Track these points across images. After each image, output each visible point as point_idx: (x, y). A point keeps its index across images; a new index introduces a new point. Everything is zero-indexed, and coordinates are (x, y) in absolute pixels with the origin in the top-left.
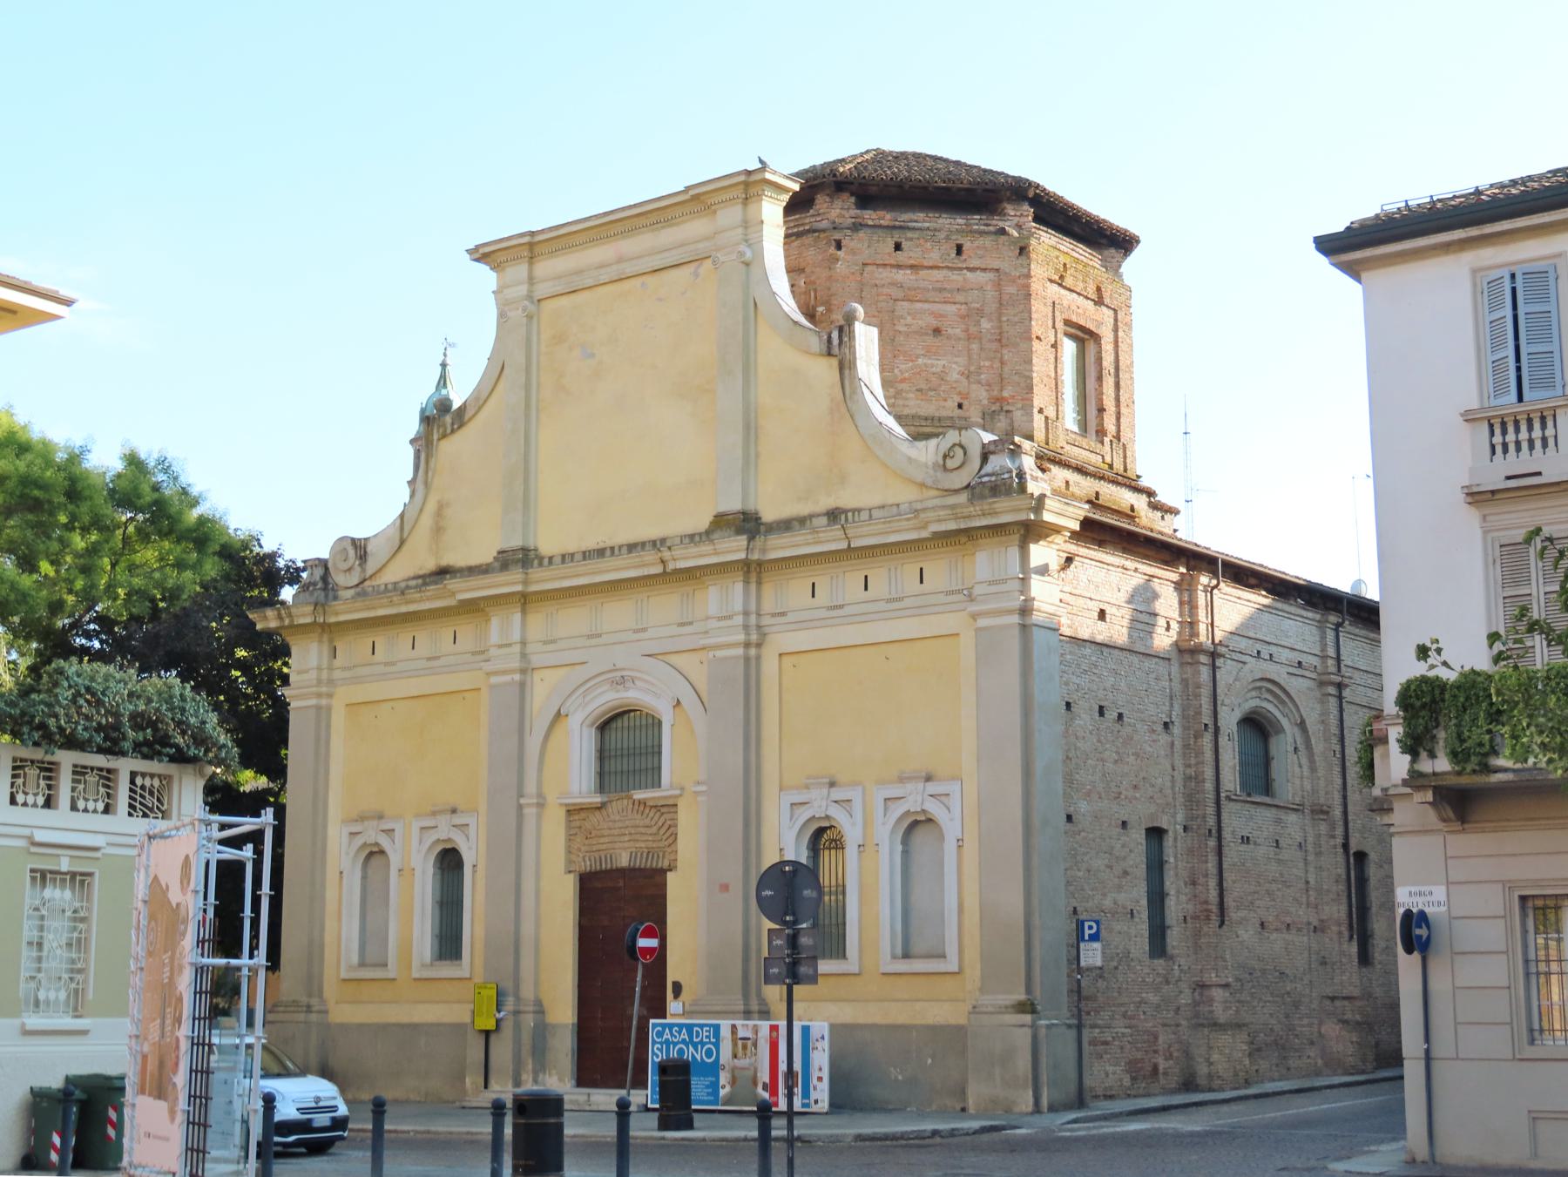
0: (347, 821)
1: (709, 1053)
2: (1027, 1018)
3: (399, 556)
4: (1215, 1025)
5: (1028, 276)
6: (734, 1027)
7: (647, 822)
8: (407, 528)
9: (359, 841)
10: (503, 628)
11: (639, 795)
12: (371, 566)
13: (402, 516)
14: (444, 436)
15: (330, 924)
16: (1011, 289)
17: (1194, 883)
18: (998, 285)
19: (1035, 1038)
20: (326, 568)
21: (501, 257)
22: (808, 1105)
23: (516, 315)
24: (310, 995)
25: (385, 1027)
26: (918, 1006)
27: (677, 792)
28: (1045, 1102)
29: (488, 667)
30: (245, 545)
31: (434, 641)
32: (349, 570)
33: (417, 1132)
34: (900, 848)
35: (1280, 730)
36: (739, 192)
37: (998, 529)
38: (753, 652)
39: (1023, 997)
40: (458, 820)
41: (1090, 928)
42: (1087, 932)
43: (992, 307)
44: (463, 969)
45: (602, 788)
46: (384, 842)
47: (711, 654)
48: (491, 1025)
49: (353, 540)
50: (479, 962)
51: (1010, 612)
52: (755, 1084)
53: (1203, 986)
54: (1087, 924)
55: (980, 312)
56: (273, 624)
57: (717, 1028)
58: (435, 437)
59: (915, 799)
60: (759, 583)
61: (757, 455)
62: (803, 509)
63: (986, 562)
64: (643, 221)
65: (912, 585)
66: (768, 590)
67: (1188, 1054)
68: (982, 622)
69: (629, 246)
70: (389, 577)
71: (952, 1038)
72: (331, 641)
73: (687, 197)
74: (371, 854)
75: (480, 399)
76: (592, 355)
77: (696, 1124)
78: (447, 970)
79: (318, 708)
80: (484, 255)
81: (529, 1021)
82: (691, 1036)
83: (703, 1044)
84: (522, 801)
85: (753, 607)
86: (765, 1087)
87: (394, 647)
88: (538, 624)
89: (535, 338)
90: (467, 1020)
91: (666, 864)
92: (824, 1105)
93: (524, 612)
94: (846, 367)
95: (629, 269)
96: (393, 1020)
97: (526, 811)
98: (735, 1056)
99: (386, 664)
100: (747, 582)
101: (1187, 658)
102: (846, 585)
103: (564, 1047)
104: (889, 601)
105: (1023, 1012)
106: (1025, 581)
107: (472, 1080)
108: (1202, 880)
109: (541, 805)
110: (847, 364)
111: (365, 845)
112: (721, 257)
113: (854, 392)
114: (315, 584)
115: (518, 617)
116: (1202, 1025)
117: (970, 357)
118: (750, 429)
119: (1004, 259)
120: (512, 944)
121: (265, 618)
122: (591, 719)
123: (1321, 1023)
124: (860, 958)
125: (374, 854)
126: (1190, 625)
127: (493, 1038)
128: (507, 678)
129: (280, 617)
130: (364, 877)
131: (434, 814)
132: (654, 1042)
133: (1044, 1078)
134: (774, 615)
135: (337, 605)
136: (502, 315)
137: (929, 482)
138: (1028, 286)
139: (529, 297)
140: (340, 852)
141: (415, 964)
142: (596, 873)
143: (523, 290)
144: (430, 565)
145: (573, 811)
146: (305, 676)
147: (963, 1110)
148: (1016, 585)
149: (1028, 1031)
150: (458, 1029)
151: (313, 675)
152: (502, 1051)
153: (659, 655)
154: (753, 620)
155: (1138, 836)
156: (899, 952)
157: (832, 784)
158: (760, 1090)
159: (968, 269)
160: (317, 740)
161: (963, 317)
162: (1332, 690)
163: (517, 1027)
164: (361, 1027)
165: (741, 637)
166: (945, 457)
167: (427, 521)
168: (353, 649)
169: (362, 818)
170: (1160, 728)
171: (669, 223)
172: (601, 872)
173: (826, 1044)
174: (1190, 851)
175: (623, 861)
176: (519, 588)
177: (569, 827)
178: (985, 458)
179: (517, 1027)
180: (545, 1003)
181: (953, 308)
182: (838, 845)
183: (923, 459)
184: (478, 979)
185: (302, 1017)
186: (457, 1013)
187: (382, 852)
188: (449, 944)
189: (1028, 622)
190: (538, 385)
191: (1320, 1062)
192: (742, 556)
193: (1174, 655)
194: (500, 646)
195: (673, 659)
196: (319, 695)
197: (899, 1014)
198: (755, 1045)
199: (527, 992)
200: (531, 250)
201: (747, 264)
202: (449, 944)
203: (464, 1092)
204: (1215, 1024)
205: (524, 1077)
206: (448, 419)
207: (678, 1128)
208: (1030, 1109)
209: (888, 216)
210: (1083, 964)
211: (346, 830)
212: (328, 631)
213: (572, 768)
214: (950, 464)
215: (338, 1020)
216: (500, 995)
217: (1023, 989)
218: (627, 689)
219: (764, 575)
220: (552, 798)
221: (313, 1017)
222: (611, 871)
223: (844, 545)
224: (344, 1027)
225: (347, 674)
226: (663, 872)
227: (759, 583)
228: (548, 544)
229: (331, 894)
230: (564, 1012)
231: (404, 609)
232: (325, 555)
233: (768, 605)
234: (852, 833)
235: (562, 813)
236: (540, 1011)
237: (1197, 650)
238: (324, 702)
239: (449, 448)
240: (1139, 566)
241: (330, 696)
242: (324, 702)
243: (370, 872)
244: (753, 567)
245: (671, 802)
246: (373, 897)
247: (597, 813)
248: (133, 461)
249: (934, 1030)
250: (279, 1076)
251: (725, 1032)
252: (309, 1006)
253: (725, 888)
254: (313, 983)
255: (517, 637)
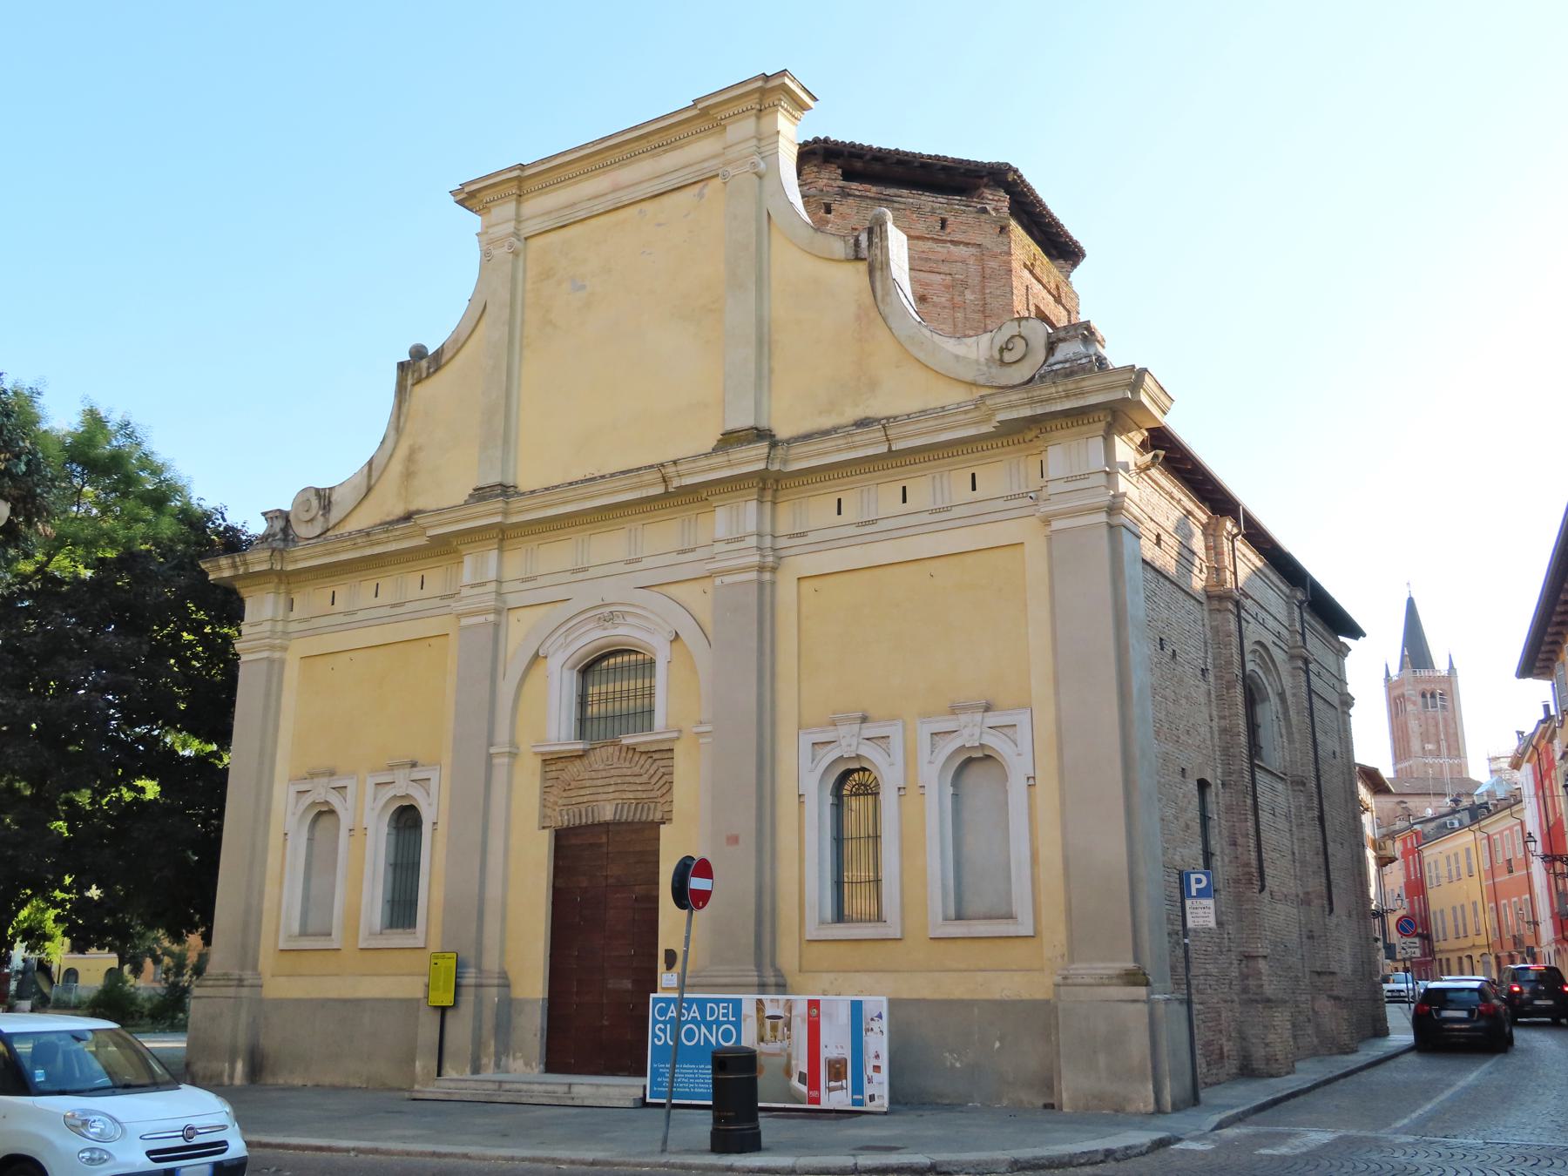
0: (294, 780)
1: (727, 1035)
2: (1141, 992)
3: (366, 503)
4: (1268, 1002)
5: (1010, 254)
6: (760, 1002)
7: (637, 770)
8: (375, 475)
9: (307, 800)
10: (479, 565)
11: (628, 740)
12: (335, 515)
13: (370, 463)
14: (419, 381)
15: (270, 889)
16: (993, 264)
17: (1235, 844)
18: (981, 260)
19: (1152, 1015)
20: (288, 521)
21: (486, 196)
22: (860, 1102)
23: (501, 252)
24: (243, 968)
25: (324, 1003)
26: (980, 977)
27: (675, 735)
28: (1167, 1098)
29: (457, 606)
30: (207, 516)
31: (399, 586)
32: (311, 520)
33: (359, 1151)
34: (950, 790)
35: (1266, 699)
36: (752, 102)
37: (1078, 416)
38: (767, 576)
39: (1131, 965)
40: (417, 774)
41: (1199, 881)
42: (1194, 887)
43: (975, 280)
44: (416, 938)
45: (581, 734)
46: (335, 801)
47: (718, 581)
48: (448, 1000)
49: (317, 490)
50: (436, 931)
51: (1096, 510)
52: (788, 1074)
53: (1249, 957)
54: (1193, 877)
55: (965, 284)
56: (227, 574)
57: (737, 1004)
58: (410, 382)
59: (971, 732)
60: (774, 503)
61: (771, 371)
62: (827, 422)
63: (1065, 457)
64: (644, 145)
65: (963, 492)
66: (784, 510)
67: (1243, 1038)
68: (1057, 525)
69: (626, 174)
70: (353, 525)
71: (1039, 1018)
72: (288, 593)
73: (695, 112)
74: (320, 814)
75: (458, 343)
76: (583, 287)
77: (765, 1139)
78: (399, 939)
79: (271, 661)
80: (470, 197)
81: (493, 995)
82: (703, 1014)
83: (719, 1024)
84: (492, 750)
85: (767, 528)
86: (802, 1078)
87: (356, 594)
88: (516, 562)
89: (520, 276)
90: (420, 994)
91: (658, 816)
92: (883, 1103)
93: (501, 549)
94: (876, 268)
95: (626, 197)
96: (333, 995)
97: (496, 761)
98: (762, 1039)
99: (346, 614)
100: (760, 501)
101: (1216, 605)
102: (882, 498)
103: (532, 1026)
104: (933, 512)
105: (1135, 984)
106: (1110, 476)
107: (423, 1065)
108: (1240, 840)
109: (513, 755)
110: (878, 265)
111: (314, 804)
112: (731, 170)
113: (887, 293)
114: (274, 535)
115: (494, 554)
116: (1257, 1001)
117: (955, 326)
118: (763, 342)
119: (988, 238)
120: (473, 910)
121: (219, 568)
122: (569, 664)
123: (1313, 999)
124: (902, 919)
125: (324, 813)
126: (1218, 570)
127: (449, 1014)
128: (481, 619)
129: (234, 566)
130: (310, 840)
131: (391, 768)
132: (656, 1022)
133: (1166, 1067)
134: (792, 536)
135: (297, 551)
136: (487, 256)
137: (981, 380)
138: (1009, 262)
139: (516, 234)
140: (286, 811)
141: (363, 932)
142: (575, 828)
143: (510, 227)
144: (399, 511)
145: (551, 761)
146: (258, 629)
147: (1049, 1106)
148: (1102, 479)
149: (1144, 1008)
150: (408, 1004)
151: (267, 626)
152: (460, 1030)
153: (655, 590)
154: (768, 542)
155: (1192, 787)
156: (952, 912)
157: (864, 719)
158: (795, 1082)
159: (952, 242)
160: (267, 695)
161: (947, 287)
162: (1300, 663)
163: (479, 1002)
164: (298, 1002)
165: (755, 559)
166: (1001, 350)
167: (396, 467)
168: (312, 600)
169: (313, 775)
170: (1199, 673)
171: (670, 146)
172: (580, 827)
173: (884, 1024)
174: (1229, 809)
175: (608, 814)
176: (498, 519)
177: (544, 779)
178: (1051, 347)
179: (479, 1002)
180: (511, 976)
181: (938, 278)
182: (870, 791)
183: (973, 355)
184: (435, 946)
185: (231, 991)
186: (409, 987)
187: (332, 812)
188: (402, 909)
189: (1116, 520)
190: (523, 322)
191: (1316, 1041)
192: (762, 466)
193: (1203, 599)
194: (473, 586)
195: (665, 589)
196: (272, 648)
197: (955, 987)
198: (788, 1025)
199: (491, 962)
200: (520, 188)
201: (760, 177)
202: (402, 909)
203: (413, 1080)
204: (1269, 1000)
205: (485, 1061)
206: (424, 363)
207: (741, 1150)
208: (1151, 1108)
209: (874, 189)
210: (1190, 924)
211: (293, 789)
212: (287, 580)
213: (549, 715)
214: (1008, 357)
215: (521, 996)
216: (460, 966)
217: (1130, 956)
218: (616, 626)
219: (780, 493)
220: (526, 746)
221: (245, 992)
222: (593, 825)
223: (884, 449)
224: (280, 1003)
225: (304, 626)
226: (655, 826)
227: (774, 503)
228: (526, 481)
229: (273, 860)
230: (532, 985)
231: (368, 552)
232: (287, 507)
233: (784, 526)
234: (889, 774)
235: (538, 762)
236: (505, 984)
237: (1224, 597)
238: (277, 655)
239: (423, 393)
240: (1184, 499)
241: (284, 649)
242: (277, 655)
243: (317, 834)
244: (770, 482)
245: (665, 747)
246: (320, 861)
247: (578, 762)
248: (95, 421)
249: (1003, 1008)
250: (127, 1088)
251: (749, 1007)
252: (241, 980)
253: (733, 840)
254: (247, 955)
255: (492, 575)
